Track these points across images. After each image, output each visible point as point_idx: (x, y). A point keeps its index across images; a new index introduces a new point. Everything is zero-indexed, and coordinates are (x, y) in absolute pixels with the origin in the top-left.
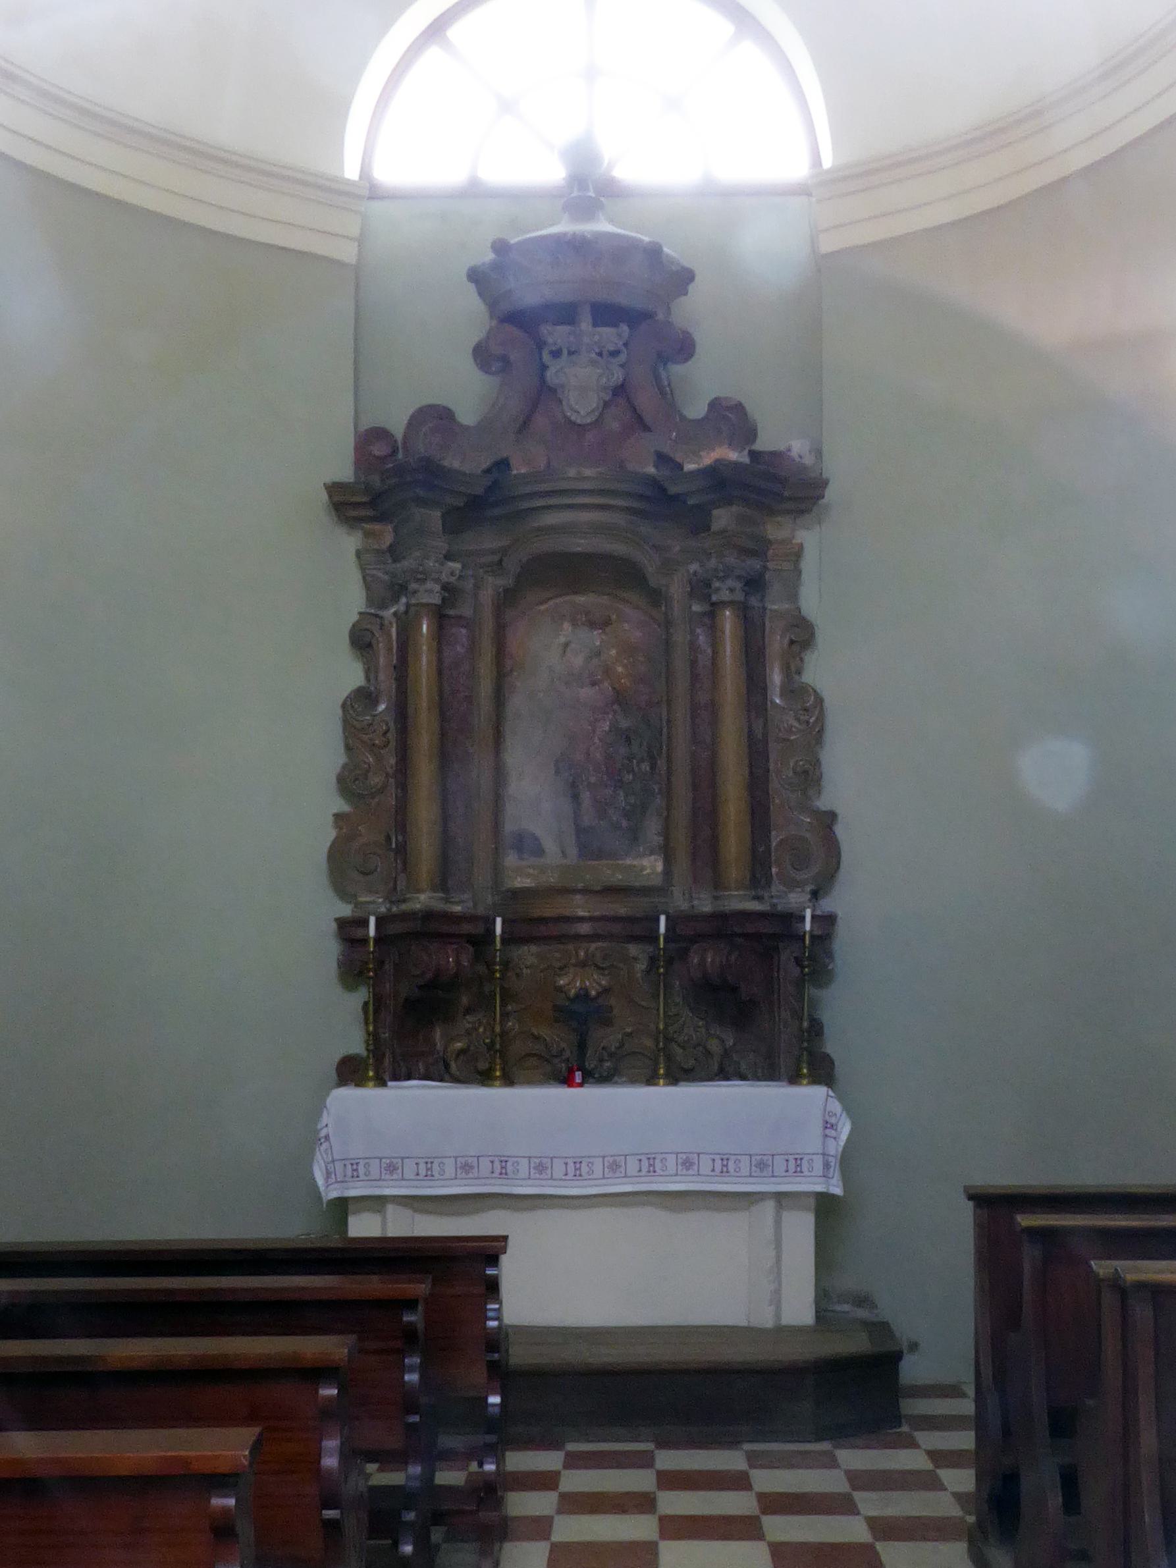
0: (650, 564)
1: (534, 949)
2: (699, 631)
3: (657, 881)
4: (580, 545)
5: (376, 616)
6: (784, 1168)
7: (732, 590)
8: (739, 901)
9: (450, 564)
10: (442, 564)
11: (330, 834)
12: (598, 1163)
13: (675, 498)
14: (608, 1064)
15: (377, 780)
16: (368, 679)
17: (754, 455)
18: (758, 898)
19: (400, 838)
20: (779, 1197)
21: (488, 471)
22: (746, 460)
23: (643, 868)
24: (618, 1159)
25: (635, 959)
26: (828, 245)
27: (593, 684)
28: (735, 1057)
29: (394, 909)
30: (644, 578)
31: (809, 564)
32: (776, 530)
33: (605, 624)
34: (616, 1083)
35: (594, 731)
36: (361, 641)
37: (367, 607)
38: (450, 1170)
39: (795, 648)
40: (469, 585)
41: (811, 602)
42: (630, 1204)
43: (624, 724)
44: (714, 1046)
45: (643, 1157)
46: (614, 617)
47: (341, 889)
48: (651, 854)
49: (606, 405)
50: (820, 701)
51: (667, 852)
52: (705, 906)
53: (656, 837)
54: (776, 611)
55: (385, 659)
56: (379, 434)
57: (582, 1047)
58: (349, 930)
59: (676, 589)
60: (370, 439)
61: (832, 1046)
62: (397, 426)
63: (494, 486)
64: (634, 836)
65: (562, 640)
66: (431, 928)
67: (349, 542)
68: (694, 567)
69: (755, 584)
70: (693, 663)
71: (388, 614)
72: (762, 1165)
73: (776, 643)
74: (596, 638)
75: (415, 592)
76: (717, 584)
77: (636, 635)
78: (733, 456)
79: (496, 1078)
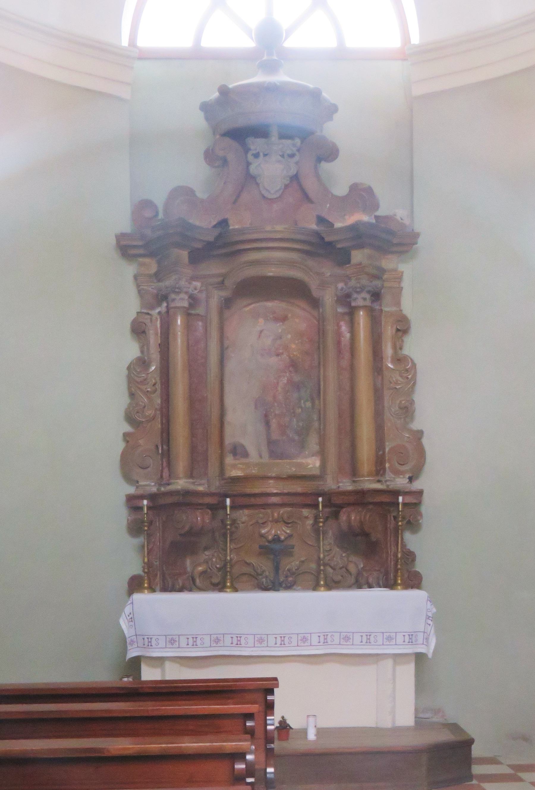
0: (313, 284)
1: (246, 512)
2: (342, 323)
3: (317, 472)
4: (271, 272)
5: (148, 314)
6: (231, 642)
7: (365, 299)
8: (370, 484)
9: (194, 283)
10: (190, 283)
11: (121, 446)
12: (294, 637)
13: (330, 244)
14: (290, 579)
15: (150, 412)
16: (142, 352)
17: (377, 217)
18: (379, 481)
19: (165, 447)
20: (395, 656)
21: (215, 226)
22: (374, 221)
23: (308, 464)
24: (263, 636)
25: (307, 518)
26: (418, 91)
27: (278, 355)
28: (365, 574)
29: (163, 489)
30: (309, 290)
31: (406, 284)
32: (388, 263)
33: (284, 319)
34: (295, 590)
35: (278, 383)
36: (138, 330)
37: (141, 308)
38: (162, 643)
39: (400, 334)
40: (203, 296)
41: (407, 306)
42: (333, 660)
43: (297, 378)
44: (352, 568)
45: (234, 636)
46: (290, 315)
47: (127, 477)
48: (313, 456)
49: (286, 186)
50: (414, 365)
51: (322, 453)
52: (347, 485)
53: (315, 446)
54: (388, 312)
55: (154, 339)
56: (146, 204)
57: (277, 569)
58: (132, 503)
59: (328, 298)
60: (142, 207)
61: (420, 567)
62: (159, 199)
63: (219, 237)
64: (302, 445)
65: (259, 328)
66: (186, 500)
67: (129, 270)
68: (341, 285)
69: (376, 296)
70: (339, 343)
71: (155, 312)
72: (347, 639)
73: (389, 331)
74: (278, 328)
75: (173, 300)
76: (355, 296)
77: (303, 326)
78: (365, 218)
79: (145, 588)
